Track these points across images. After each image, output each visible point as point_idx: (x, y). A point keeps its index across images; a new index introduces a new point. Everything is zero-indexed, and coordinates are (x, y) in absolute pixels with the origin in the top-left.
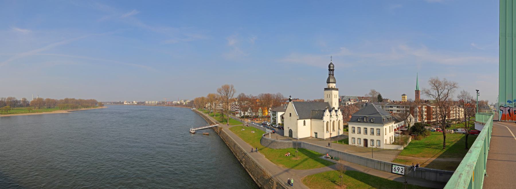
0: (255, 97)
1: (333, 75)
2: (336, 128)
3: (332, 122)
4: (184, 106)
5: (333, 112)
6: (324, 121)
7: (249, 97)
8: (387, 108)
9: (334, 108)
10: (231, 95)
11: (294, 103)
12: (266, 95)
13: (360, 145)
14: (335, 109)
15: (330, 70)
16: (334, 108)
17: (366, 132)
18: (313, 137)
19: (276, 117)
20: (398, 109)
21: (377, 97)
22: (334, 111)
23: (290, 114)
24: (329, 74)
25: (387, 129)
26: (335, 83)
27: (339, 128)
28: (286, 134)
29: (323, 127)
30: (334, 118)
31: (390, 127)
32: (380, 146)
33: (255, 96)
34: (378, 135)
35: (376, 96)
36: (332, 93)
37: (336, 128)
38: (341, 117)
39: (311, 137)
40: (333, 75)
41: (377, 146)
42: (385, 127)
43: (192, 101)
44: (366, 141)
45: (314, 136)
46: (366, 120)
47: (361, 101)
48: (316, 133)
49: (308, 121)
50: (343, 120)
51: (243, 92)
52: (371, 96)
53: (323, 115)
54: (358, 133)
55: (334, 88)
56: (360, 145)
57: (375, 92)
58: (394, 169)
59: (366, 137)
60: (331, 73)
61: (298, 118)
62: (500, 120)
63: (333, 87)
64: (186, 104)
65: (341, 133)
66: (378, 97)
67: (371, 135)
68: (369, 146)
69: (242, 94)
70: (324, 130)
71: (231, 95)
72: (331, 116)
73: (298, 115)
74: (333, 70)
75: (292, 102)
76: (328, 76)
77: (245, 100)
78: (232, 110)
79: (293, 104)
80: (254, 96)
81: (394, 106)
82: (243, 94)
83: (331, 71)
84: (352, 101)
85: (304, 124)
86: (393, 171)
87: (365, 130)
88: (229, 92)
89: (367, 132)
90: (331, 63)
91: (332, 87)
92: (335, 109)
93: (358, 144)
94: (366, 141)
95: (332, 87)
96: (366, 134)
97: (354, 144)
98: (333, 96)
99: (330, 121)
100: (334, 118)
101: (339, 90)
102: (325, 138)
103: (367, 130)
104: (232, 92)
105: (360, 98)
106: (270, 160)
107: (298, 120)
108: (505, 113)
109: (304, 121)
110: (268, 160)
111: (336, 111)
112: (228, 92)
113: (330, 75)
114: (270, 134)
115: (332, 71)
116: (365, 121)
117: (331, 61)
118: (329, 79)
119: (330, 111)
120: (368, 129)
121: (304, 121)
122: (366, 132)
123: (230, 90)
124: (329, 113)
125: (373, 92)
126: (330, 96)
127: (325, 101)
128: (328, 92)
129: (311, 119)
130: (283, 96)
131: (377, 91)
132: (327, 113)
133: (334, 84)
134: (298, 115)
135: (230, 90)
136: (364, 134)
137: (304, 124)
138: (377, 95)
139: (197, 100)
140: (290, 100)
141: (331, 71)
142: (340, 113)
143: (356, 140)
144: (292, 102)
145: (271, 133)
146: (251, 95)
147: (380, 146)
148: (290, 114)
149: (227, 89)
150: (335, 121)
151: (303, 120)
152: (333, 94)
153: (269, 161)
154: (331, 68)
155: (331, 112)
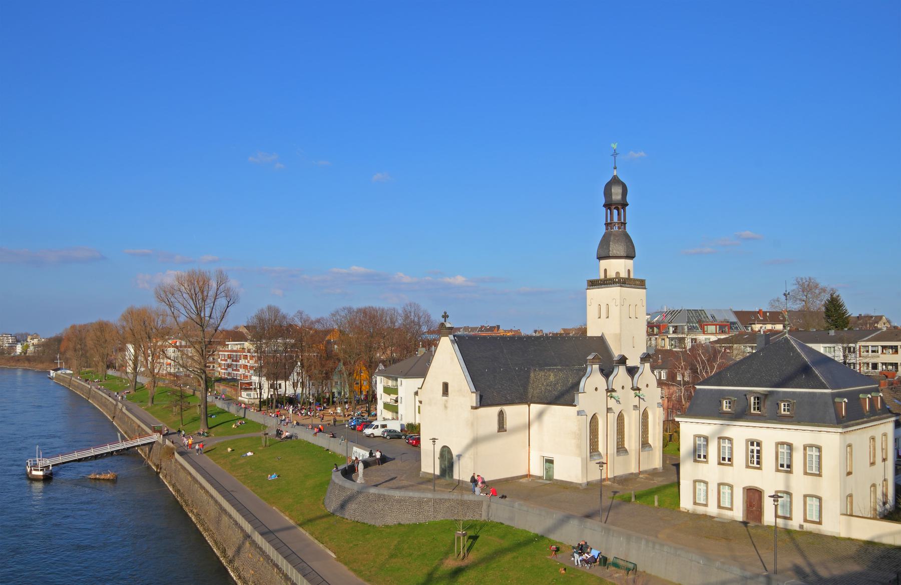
0: (318, 321)
2: (632, 441)
3: (612, 417)
4: (18, 359)
5: (620, 375)
7: (293, 319)
8: (866, 357)
9: (623, 360)
10: (217, 314)
12: (364, 312)
14: (629, 363)
15: (608, 206)
17: (755, 459)
19: (396, 401)
21: (823, 309)
23: (446, 386)
24: (607, 224)
27: (645, 444)
28: (430, 465)
31: (873, 438)
32: (820, 523)
33: (319, 317)
35: (819, 304)
37: (632, 441)
38: (653, 395)
41: (806, 520)
43: (58, 340)
44: (754, 497)
51: (274, 303)
52: (796, 306)
57: (816, 287)
59: (754, 479)
60: (615, 219)
62: (718, 332)
64: (25, 351)
65: (656, 462)
66: (827, 310)
69: (270, 308)
71: (217, 314)
72: (610, 391)
74: (624, 205)
76: (603, 230)
77: (714, 356)
78: (229, 374)
80: (313, 317)
82: (275, 311)
83: (615, 212)
84: (712, 329)
87: (752, 451)
88: (208, 301)
89: (758, 457)
90: (615, 181)
91: (618, 273)
92: (629, 363)
93: (719, 507)
94: (754, 497)
97: (701, 510)
103: (758, 452)
104: (222, 302)
105: (746, 317)
106: (355, 571)
108: (486, 519)
109: (501, 414)
110: (345, 568)
111: (632, 371)
112: (204, 300)
114: (361, 467)
115: (617, 209)
116: (783, 412)
117: (615, 168)
118: (605, 242)
119: (606, 373)
120: (764, 445)
121: (501, 414)
122: (755, 459)
123: (212, 293)
124: (630, 378)
125: (808, 288)
127: (590, 333)
130: (429, 316)
131: (823, 284)
132: (593, 381)
135: (212, 293)
136: (747, 467)
138: (826, 297)
139: (78, 335)
141: (615, 212)
142: (648, 377)
145: (366, 464)
146: (300, 313)
147: (820, 523)
148: (446, 386)
149: (197, 289)
151: (495, 410)
153: (352, 574)
155: (611, 378)
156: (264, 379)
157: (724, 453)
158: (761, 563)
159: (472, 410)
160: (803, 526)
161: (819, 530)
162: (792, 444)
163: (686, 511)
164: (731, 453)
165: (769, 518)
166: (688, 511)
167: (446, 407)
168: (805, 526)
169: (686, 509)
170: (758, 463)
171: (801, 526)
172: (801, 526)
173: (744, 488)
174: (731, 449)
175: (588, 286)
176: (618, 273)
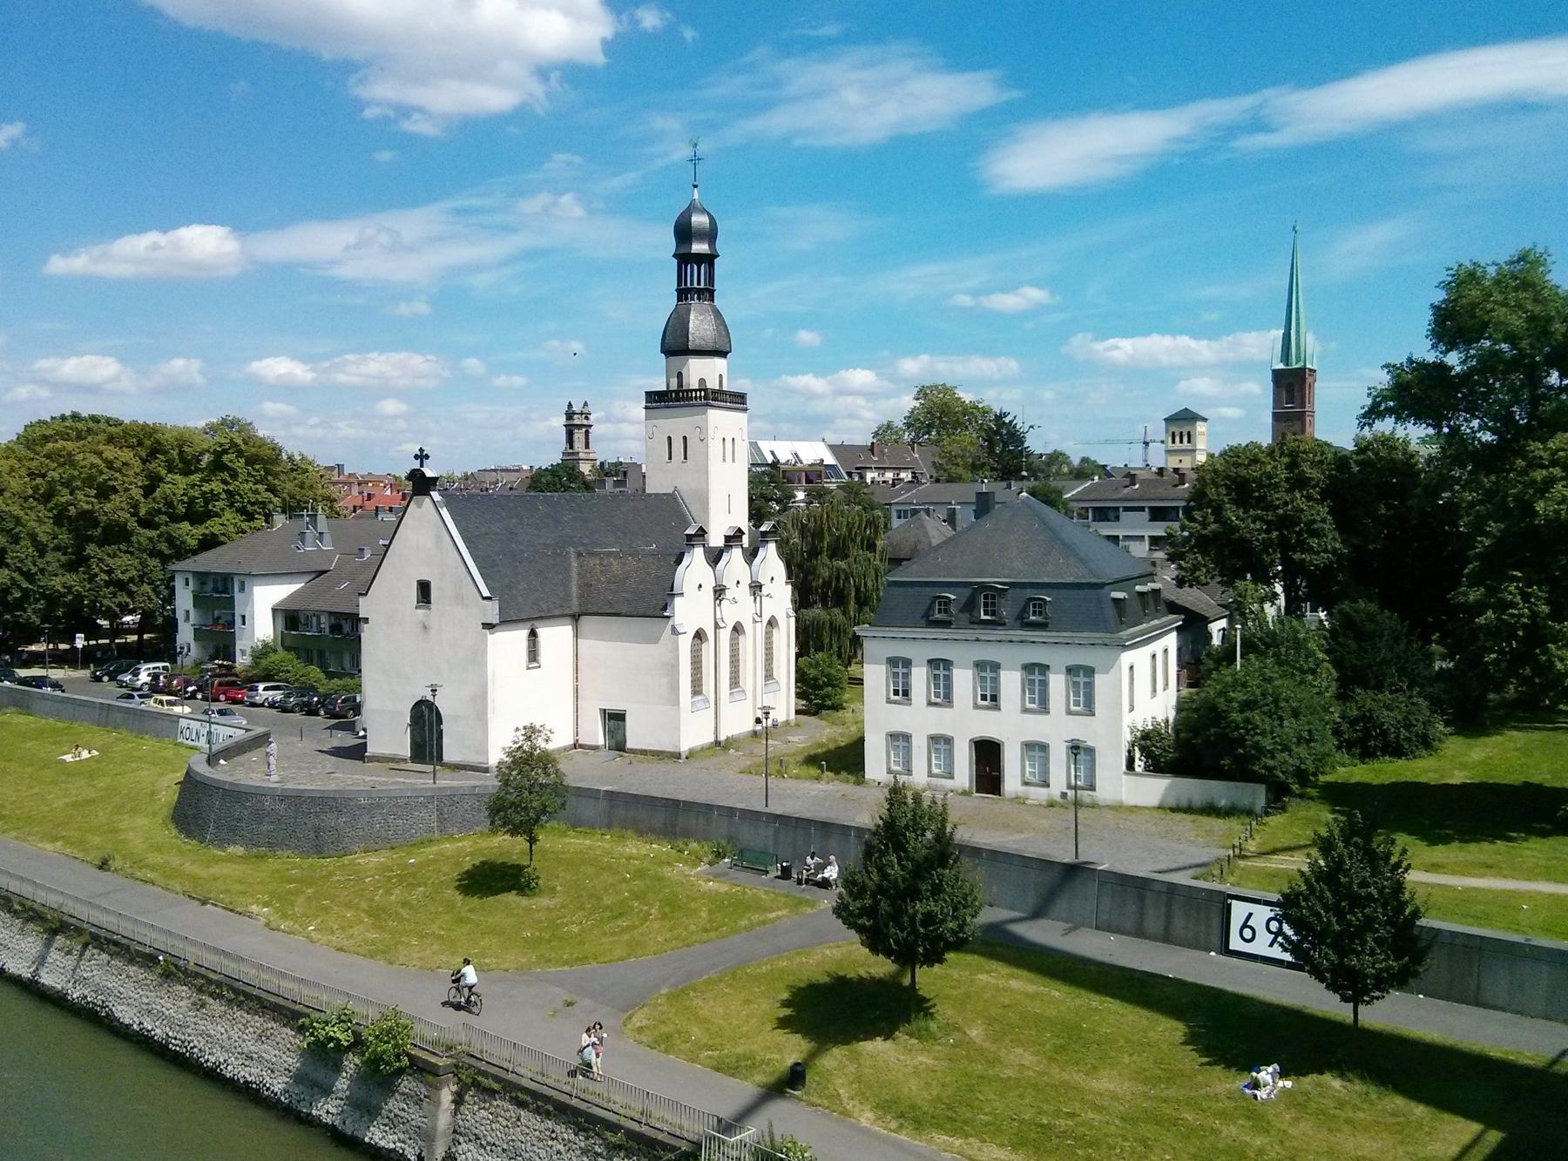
1: (712, 292)
6: (675, 631)
11: (451, 500)
13: (948, 783)
16: (702, 532)
18: (595, 748)
20: (1159, 530)
22: (698, 552)
25: (1135, 669)
26: (723, 354)
29: (674, 668)
30: (739, 607)
31: (1154, 656)
34: (895, 702)
36: (702, 429)
38: (780, 597)
39: (576, 746)
40: (708, 293)
42: (1127, 658)
44: (988, 754)
45: (596, 734)
46: (993, 613)
47: (862, 477)
48: (615, 719)
49: (556, 636)
50: (793, 620)
53: (669, 593)
54: (930, 704)
55: (721, 392)
56: (948, 783)
58: (1245, 926)
59: (989, 725)
61: (492, 612)
63: (713, 384)
67: (1027, 716)
68: (1012, 781)
70: (674, 688)
72: (719, 592)
73: (486, 593)
75: (435, 495)
79: (445, 512)
81: (1127, 509)
85: (533, 655)
86: (1236, 943)
91: (702, 381)
94: (988, 754)
95: (702, 381)
96: (987, 708)
98: (715, 448)
99: (717, 626)
100: (739, 607)
101: (749, 403)
102: (685, 748)
107: (489, 626)
113: (683, 294)
116: (983, 617)
126: (684, 449)
128: (677, 423)
129: (575, 618)
133: (719, 363)
134: (486, 593)
137: (533, 655)
140: (421, 484)
143: (914, 750)
144: (435, 495)
150: (748, 626)
152: (711, 432)
154: (699, 247)
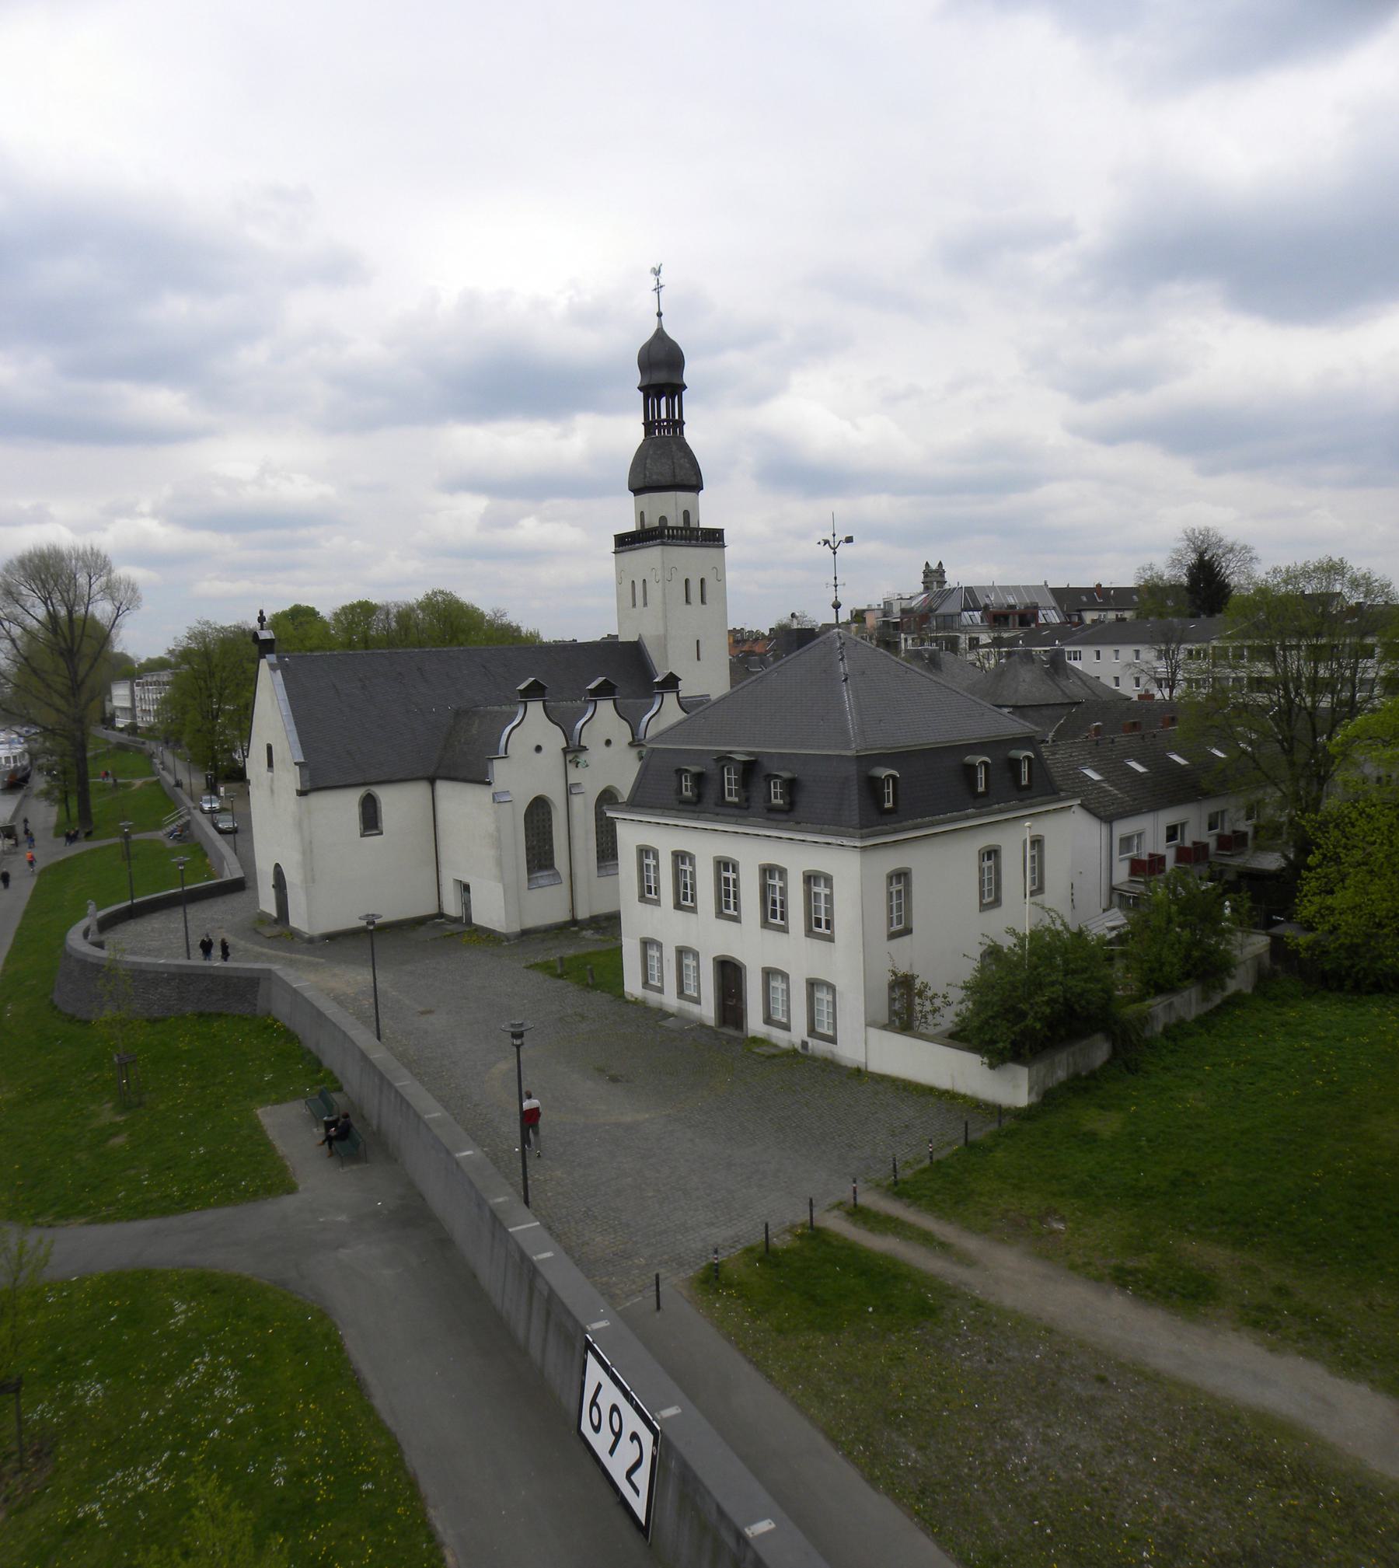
91: (663, 519)
120: (741, 870)
156: (1053, 928)
157: (817, 909)
158: (521, 1056)
159: (303, 798)
160: (807, 1043)
161: (831, 1052)
162: (1000, 905)
163: (633, 999)
164: (830, 911)
165: (755, 1023)
166: (636, 999)
167: (272, 791)
168: (810, 1045)
169: (632, 996)
170: (736, 907)
171: (805, 1044)
172: (805, 1044)
173: (714, 959)
174: (829, 899)
175: (965, 588)
176: (663, 519)
